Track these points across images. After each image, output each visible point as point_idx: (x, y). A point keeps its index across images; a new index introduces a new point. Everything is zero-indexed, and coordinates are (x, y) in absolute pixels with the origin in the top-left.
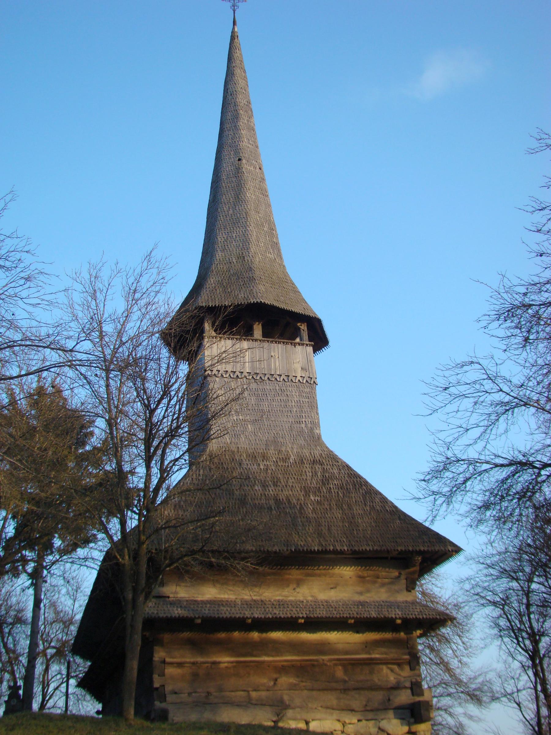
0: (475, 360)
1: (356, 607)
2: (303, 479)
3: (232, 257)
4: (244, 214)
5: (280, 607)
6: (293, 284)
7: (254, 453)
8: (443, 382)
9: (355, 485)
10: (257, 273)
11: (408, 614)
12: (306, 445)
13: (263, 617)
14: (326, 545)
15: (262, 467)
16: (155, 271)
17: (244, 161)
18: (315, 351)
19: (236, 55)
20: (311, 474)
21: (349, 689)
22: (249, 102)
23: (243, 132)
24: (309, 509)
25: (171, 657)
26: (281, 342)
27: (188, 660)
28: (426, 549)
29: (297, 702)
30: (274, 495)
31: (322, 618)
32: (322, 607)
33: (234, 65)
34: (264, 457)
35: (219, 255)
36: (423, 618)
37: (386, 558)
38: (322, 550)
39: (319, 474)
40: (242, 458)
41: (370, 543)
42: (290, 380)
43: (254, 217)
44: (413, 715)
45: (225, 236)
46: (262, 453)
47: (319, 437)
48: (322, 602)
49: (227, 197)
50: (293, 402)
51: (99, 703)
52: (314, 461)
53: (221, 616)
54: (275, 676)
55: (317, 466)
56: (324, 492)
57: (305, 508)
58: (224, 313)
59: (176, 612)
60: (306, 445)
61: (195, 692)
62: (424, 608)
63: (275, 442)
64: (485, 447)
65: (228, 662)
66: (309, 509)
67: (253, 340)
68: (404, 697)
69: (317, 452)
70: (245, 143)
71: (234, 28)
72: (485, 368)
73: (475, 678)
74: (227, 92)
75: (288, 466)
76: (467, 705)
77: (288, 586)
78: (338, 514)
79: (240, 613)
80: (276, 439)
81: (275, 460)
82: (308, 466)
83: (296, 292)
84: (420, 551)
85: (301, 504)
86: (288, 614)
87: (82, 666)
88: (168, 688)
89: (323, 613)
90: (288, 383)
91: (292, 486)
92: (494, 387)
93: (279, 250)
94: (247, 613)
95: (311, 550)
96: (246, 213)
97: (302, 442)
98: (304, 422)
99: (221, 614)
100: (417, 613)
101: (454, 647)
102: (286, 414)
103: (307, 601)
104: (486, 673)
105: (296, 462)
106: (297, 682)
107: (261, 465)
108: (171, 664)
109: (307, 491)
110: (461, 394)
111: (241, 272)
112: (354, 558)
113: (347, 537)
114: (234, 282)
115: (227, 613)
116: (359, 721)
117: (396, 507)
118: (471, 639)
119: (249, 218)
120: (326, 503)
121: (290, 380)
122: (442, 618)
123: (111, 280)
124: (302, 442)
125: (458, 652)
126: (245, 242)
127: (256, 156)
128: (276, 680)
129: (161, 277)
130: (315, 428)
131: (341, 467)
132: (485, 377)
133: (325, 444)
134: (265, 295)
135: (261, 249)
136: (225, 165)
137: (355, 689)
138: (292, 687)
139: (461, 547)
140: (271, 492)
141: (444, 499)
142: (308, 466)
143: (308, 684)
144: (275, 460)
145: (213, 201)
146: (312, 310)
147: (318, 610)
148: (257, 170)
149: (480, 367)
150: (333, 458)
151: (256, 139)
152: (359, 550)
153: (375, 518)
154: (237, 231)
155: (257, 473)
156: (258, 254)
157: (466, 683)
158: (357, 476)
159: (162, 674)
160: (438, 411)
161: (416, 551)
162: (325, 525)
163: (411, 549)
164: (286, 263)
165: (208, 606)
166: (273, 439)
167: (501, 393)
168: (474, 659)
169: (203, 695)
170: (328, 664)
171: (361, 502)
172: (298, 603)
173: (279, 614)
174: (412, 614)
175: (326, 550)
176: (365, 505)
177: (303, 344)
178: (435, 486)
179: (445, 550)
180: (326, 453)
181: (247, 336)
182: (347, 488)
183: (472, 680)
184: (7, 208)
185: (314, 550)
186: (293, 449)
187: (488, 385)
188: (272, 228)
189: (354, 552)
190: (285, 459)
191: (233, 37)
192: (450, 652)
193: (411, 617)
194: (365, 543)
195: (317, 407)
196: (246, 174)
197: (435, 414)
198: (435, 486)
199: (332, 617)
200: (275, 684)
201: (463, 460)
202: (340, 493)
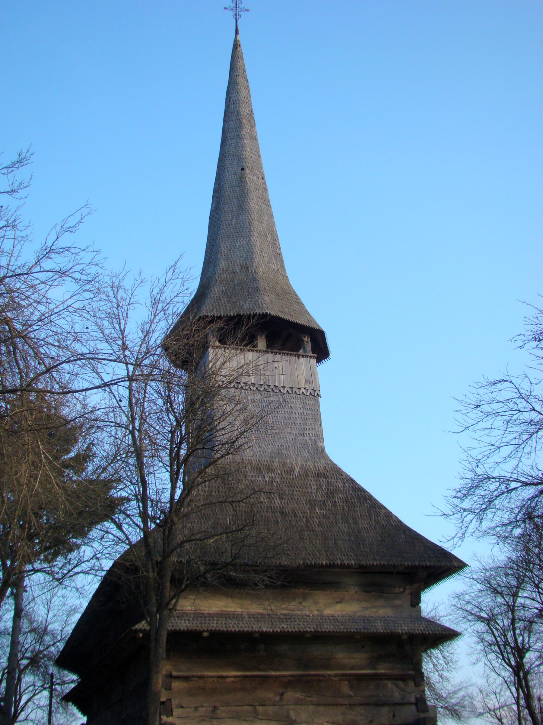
0: (507, 378)
1: (362, 622)
2: (308, 492)
3: (236, 266)
4: (248, 224)
5: (287, 621)
6: (296, 295)
7: (258, 464)
8: (474, 399)
9: (359, 499)
10: (262, 284)
11: (414, 630)
12: (310, 458)
13: (271, 631)
14: (333, 559)
15: (267, 479)
16: (179, 282)
17: (247, 171)
18: (318, 362)
19: (239, 64)
20: (315, 487)
22: (252, 112)
23: (246, 142)
24: (315, 523)
25: (177, 671)
26: (284, 353)
27: (195, 674)
30: (280, 507)
32: (329, 621)
33: (237, 74)
34: (269, 469)
35: (223, 264)
36: (429, 633)
37: (392, 573)
38: (330, 564)
39: (324, 487)
40: (247, 469)
41: (377, 558)
42: (294, 392)
43: (257, 227)
45: (229, 246)
46: (266, 465)
47: (323, 450)
48: (328, 616)
49: (231, 207)
50: (297, 414)
51: (84, 715)
52: (318, 473)
53: (230, 630)
54: (281, 691)
55: (322, 479)
56: (329, 505)
57: (311, 522)
58: (248, 324)
59: (184, 625)
60: (310, 458)
61: (202, 706)
62: (429, 623)
63: (279, 453)
64: (518, 465)
65: (235, 677)
66: (315, 523)
67: (257, 351)
69: (321, 465)
70: (248, 153)
71: (236, 37)
72: (517, 386)
73: (455, 692)
74: (230, 101)
75: (293, 478)
76: (446, 720)
77: (294, 599)
78: (343, 527)
79: (248, 627)
80: (280, 451)
81: (279, 472)
82: (312, 479)
83: (300, 303)
84: (427, 566)
85: (306, 517)
86: (296, 627)
87: (70, 679)
88: (175, 702)
89: (330, 628)
90: (292, 395)
91: (298, 499)
92: (527, 406)
93: (282, 261)
94: (254, 627)
95: (319, 564)
96: (250, 223)
97: (306, 455)
98: (308, 435)
99: (230, 627)
100: (422, 629)
101: (435, 661)
102: (290, 427)
103: (314, 616)
104: (466, 687)
105: (300, 475)
106: (303, 697)
107: (266, 477)
108: (178, 678)
109: (312, 504)
110: (494, 412)
111: (245, 282)
112: (358, 572)
113: (354, 551)
114: (239, 293)
115: (235, 626)
117: (400, 522)
118: (452, 654)
119: (252, 228)
120: (332, 516)
121: (294, 392)
122: (447, 633)
123: (134, 289)
124: (306, 455)
125: (438, 666)
126: (249, 252)
127: (259, 167)
128: (282, 694)
129: (185, 288)
130: (318, 441)
131: (345, 481)
132: (518, 395)
133: (329, 458)
134: (271, 306)
135: (265, 259)
136: (227, 175)
138: (298, 702)
139: (467, 563)
140: (277, 505)
141: (474, 516)
142: (312, 479)
143: (315, 699)
144: (279, 472)
145: (216, 210)
146: (315, 322)
147: (325, 624)
148: (260, 180)
149: (513, 386)
150: (338, 471)
151: (259, 149)
152: (366, 564)
153: (380, 532)
154: (241, 240)
155: (262, 485)
156: (261, 264)
157: (445, 698)
159: (168, 688)
160: (470, 428)
161: (423, 566)
162: (331, 539)
163: (417, 564)
164: (289, 274)
165: (216, 619)
166: (277, 451)
167: (533, 411)
168: (454, 674)
169: (210, 709)
170: (334, 679)
171: (366, 516)
172: (305, 617)
173: (287, 628)
174: (418, 630)
175: (334, 564)
176: (370, 519)
177: (306, 356)
178: (466, 504)
179: (451, 565)
180: (330, 466)
181: (272, 349)
182: (352, 502)
183: (451, 695)
184: (82, 221)
185: (322, 564)
186: (298, 461)
187: (522, 404)
188: (275, 239)
189: (361, 566)
190: (290, 471)
191: (236, 45)
192: (431, 666)
193: (418, 632)
194: (372, 558)
195: (320, 420)
196: (249, 184)
197: (467, 431)
198: (466, 504)
199: (340, 632)
200: (281, 699)
201: (493, 478)
202: (345, 506)
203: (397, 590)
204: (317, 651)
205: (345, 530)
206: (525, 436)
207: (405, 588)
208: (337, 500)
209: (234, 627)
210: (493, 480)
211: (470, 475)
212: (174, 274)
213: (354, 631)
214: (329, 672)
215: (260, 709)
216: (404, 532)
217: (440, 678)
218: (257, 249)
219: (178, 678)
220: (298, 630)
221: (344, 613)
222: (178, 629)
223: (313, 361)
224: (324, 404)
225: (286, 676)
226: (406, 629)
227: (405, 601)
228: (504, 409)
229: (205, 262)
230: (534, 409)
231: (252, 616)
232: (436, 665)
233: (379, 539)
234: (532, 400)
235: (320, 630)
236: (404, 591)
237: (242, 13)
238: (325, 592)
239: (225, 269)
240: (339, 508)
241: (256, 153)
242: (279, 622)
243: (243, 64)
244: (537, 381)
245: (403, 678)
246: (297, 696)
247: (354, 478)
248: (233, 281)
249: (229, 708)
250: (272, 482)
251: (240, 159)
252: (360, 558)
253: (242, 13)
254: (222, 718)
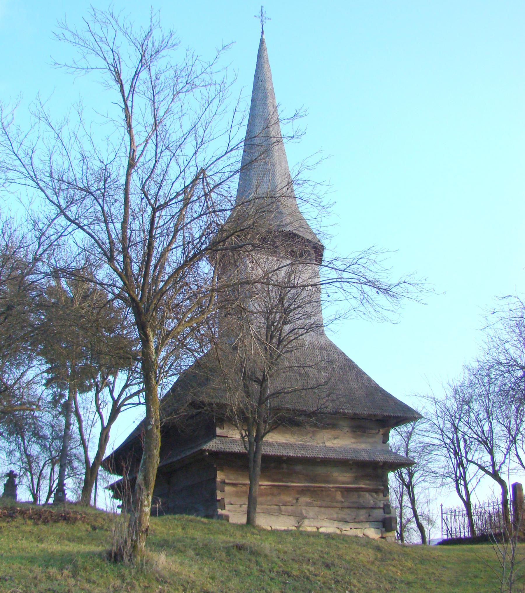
21: (344, 508)
27: (240, 482)
28: (402, 415)
29: (311, 514)
31: (331, 458)
44: (384, 526)
54: (297, 496)
55: (324, 351)
68: (379, 514)
71: (262, 36)
88: (226, 501)
108: (228, 484)
128: (297, 499)
138: (308, 505)
143: (319, 503)
158: (350, 361)
159: (223, 491)
163: (392, 414)
191: (262, 42)
200: (297, 502)
203: (374, 431)
204: (321, 470)
207: (379, 431)
215: (283, 508)
219: (228, 484)
221: (339, 446)
225: (299, 487)
227: (379, 438)
231: (280, 445)
233: (365, 396)
236: (378, 433)
237: (266, 21)
238: (327, 431)
245: (376, 491)
249: (263, 506)
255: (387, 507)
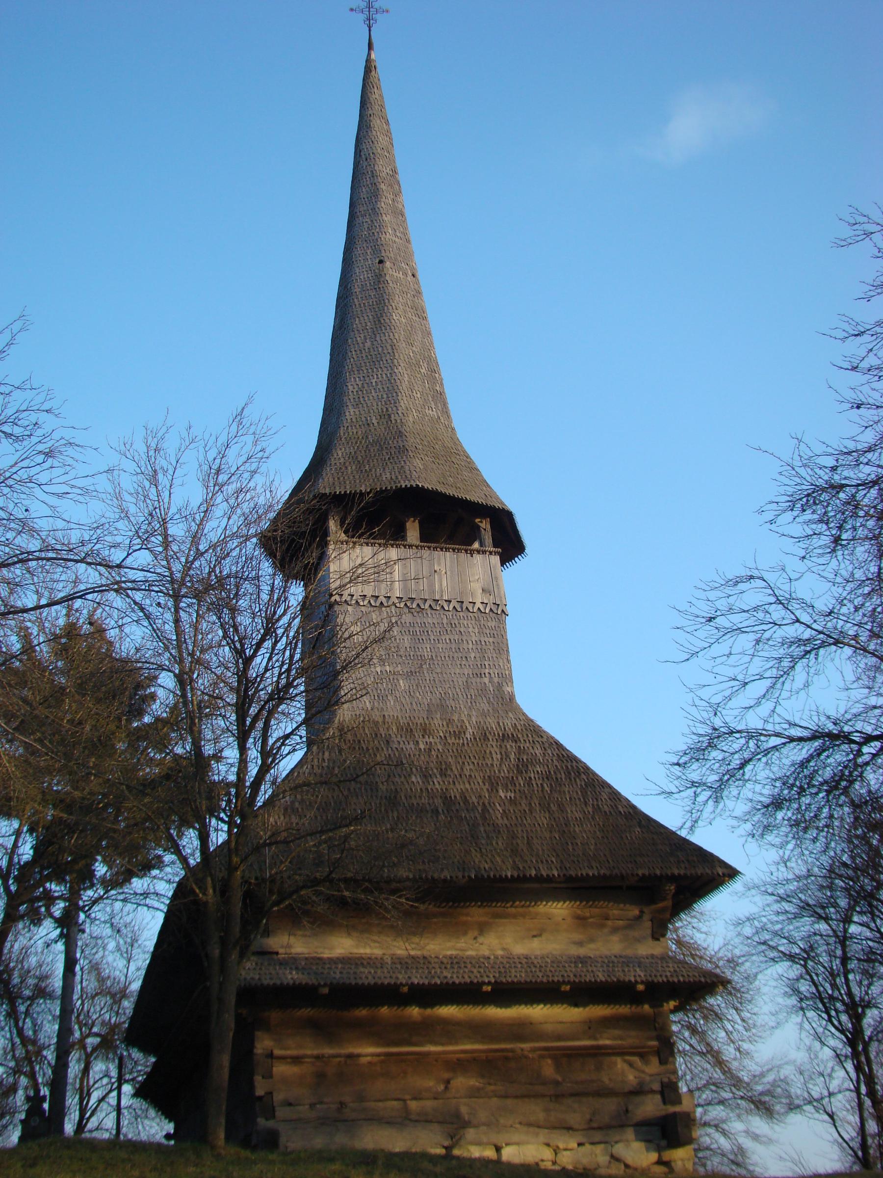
0: (756, 573)
2: (487, 764)
4: (389, 347)
5: (453, 968)
6: (468, 457)
7: (408, 724)
8: (706, 608)
10: (411, 441)
11: (656, 976)
14: (524, 867)
15: (422, 746)
16: (249, 439)
17: (388, 264)
19: (374, 96)
20: (499, 756)
21: (563, 1096)
22: (395, 171)
24: (497, 812)
25: (281, 1049)
26: (449, 549)
27: (309, 1052)
28: (682, 872)
30: (442, 789)
31: (519, 983)
32: (519, 966)
34: (426, 731)
35: (350, 413)
36: (679, 981)
38: (518, 876)
39: (512, 756)
40: (391, 732)
41: (594, 864)
42: (464, 608)
46: (421, 724)
47: (512, 698)
49: (363, 321)
50: (470, 642)
51: (170, 1121)
52: (503, 735)
53: (360, 982)
54: (446, 1075)
55: (509, 745)
56: (520, 784)
57: (491, 811)
59: (289, 977)
61: (321, 1103)
62: (680, 965)
63: (442, 706)
65: (372, 1055)
68: (650, 1107)
70: (389, 236)
71: (369, 55)
72: (772, 585)
73: (762, 1075)
74: (360, 156)
75: (463, 744)
76: (750, 1117)
77: (465, 933)
78: (543, 819)
79: (391, 977)
80: (443, 702)
81: (442, 734)
82: (494, 744)
83: (473, 469)
85: (484, 804)
86: (466, 977)
87: (142, 1062)
88: (278, 1097)
89: (521, 976)
90: (461, 614)
91: (470, 776)
93: (445, 404)
94: (400, 976)
95: (500, 876)
97: (485, 706)
98: (487, 675)
100: (668, 974)
103: (496, 957)
105: (475, 739)
106: (481, 1085)
109: (493, 783)
110: (735, 627)
111: (386, 439)
112: (566, 888)
113: (558, 855)
115: (370, 977)
116: (579, 1145)
117: (634, 807)
118: (754, 1014)
119: (396, 354)
121: (464, 608)
122: (709, 981)
124: (485, 706)
125: (735, 1034)
126: (392, 391)
127: (407, 255)
128: (448, 1082)
129: (259, 448)
130: (504, 684)
131: (547, 745)
132: (772, 599)
133: (521, 709)
134: (424, 474)
135: (417, 402)
136: (357, 271)
137: (572, 1095)
138: (474, 1093)
140: (437, 786)
142: (494, 744)
144: (442, 734)
145: (341, 328)
146: (497, 498)
148: (409, 278)
149: (764, 584)
150: (534, 730)
151: (406, 229)
152: (577, 875)
153: (601, 824)
155: (414, 755)
156: (412, 410)
157: (748, 1084)
158: (572, 759)
159: (268, 1075)
160: (699, 655)
161: (667, 875)
162: (523, 837)
163: (658, 872)
164: (456, 424)
165: (340, 966)
166: (438, 701)
167: (797, 624)
168: (759, 1046)
171: (579, 799)
172: (482, 960)
173: (452, 977)
174: (661, 976)
175: (525, 876)
176: (586, 804)
177: (484, 552)
179: (713, 873)
180: (522, 723)
181: (396, 540)
182: (557, 778)
185: (506, 876)
186: (470, 718)
187: (777, 613)
189: (569, 879)
191: (369, 68)
192: (723, 1034)
193: (660, 980)
194: (586, 864)
195: (508, 651)
196: (391, 284)
197: (695, 659)
198: (695, 772)
199: (536, 982)
200: (446, 1088)
205: (545, 822)
206: (786, 663)
208: (532, 776)
209: (367, 978)
210: (737, 735)
211: (703, 730)
212: (241, 427)
213: (558, 981)
214: (523, 1046)
216: (640, 825)
217: (738, 1054)
218: (404, 386)
220: (468, 981)
222: (278, 982)
223: (496, 560)
224: (513, 627)
226: (642, 974)
228: (750, 622)
229: (325, 410)
230: (798, 621)
232: (731, 1033)
234: (794, 606)
235: (504, 980)
237: (378, 17)
239: (354, 420)
240: (536, 788)
241: (402, 236)
242: (440, 968)
243: (381, 96)
244: (797, 575)
246: (472, 1083)
247: (562, 741)
248: (367, 437)
250: (430, 750)
251: (377, 248)
252: (568, 865)
253: (378, 17)
254: (353, 1120)
255: (669, 1091)
